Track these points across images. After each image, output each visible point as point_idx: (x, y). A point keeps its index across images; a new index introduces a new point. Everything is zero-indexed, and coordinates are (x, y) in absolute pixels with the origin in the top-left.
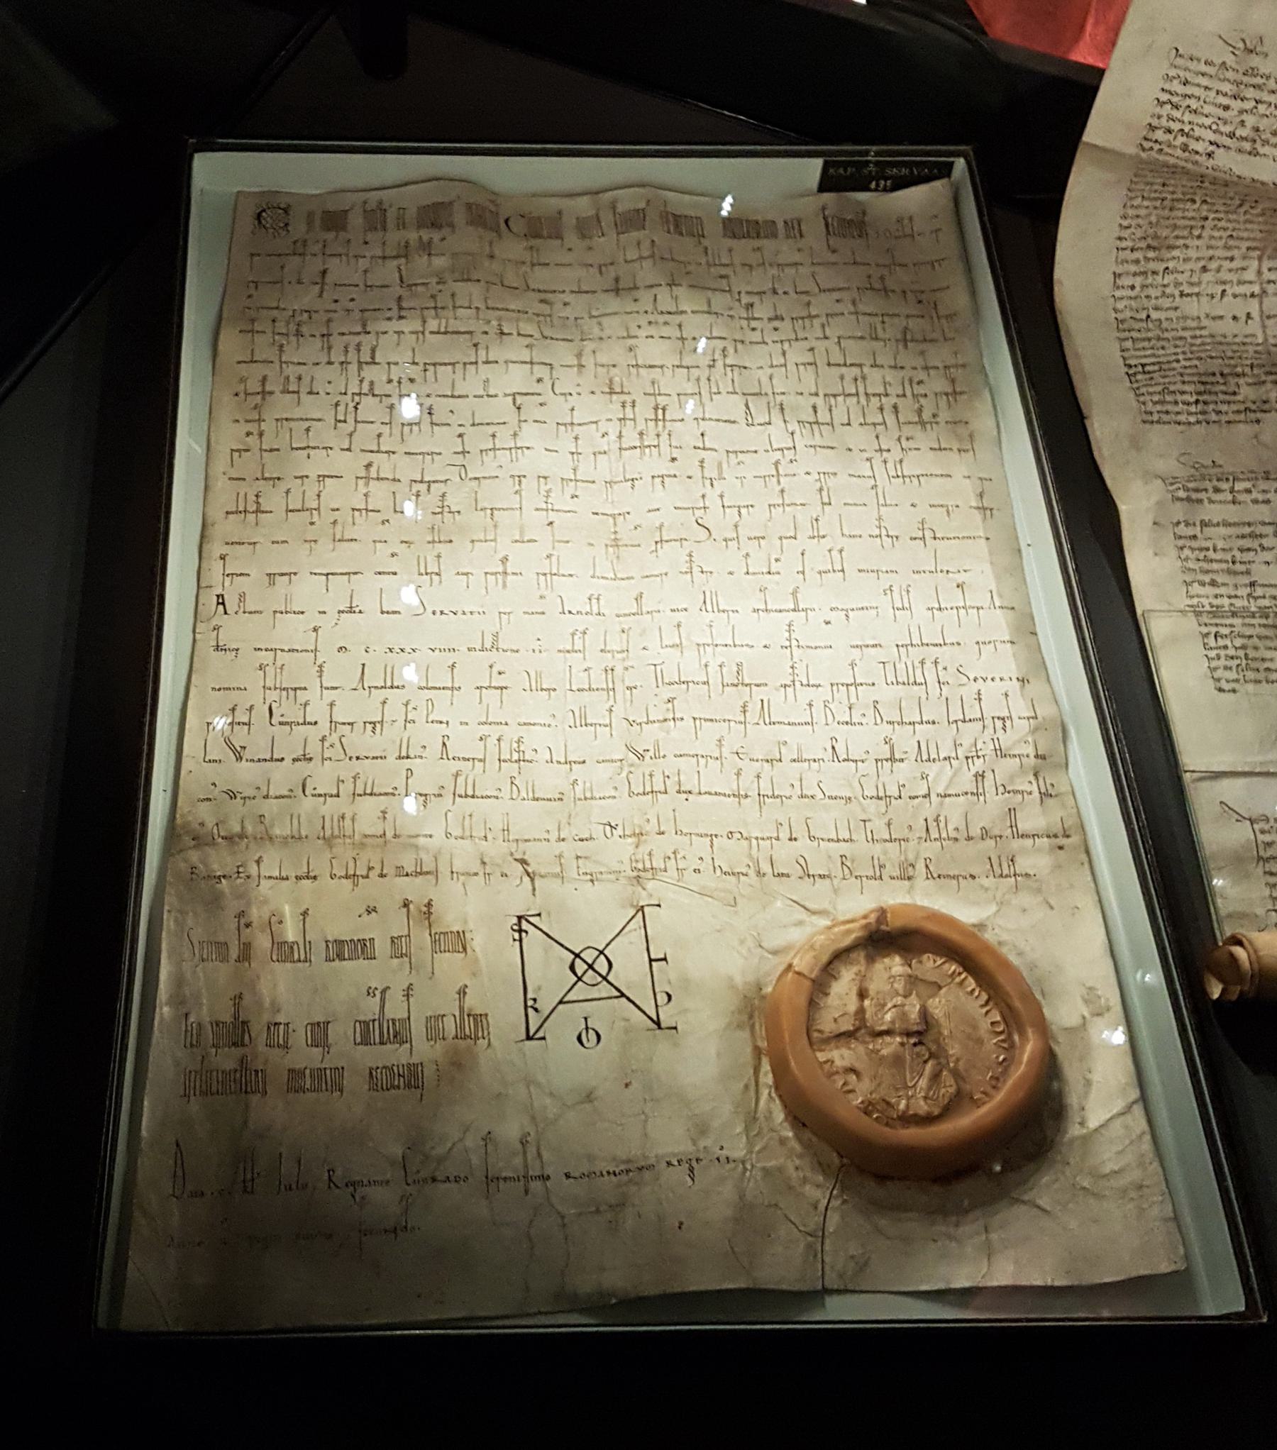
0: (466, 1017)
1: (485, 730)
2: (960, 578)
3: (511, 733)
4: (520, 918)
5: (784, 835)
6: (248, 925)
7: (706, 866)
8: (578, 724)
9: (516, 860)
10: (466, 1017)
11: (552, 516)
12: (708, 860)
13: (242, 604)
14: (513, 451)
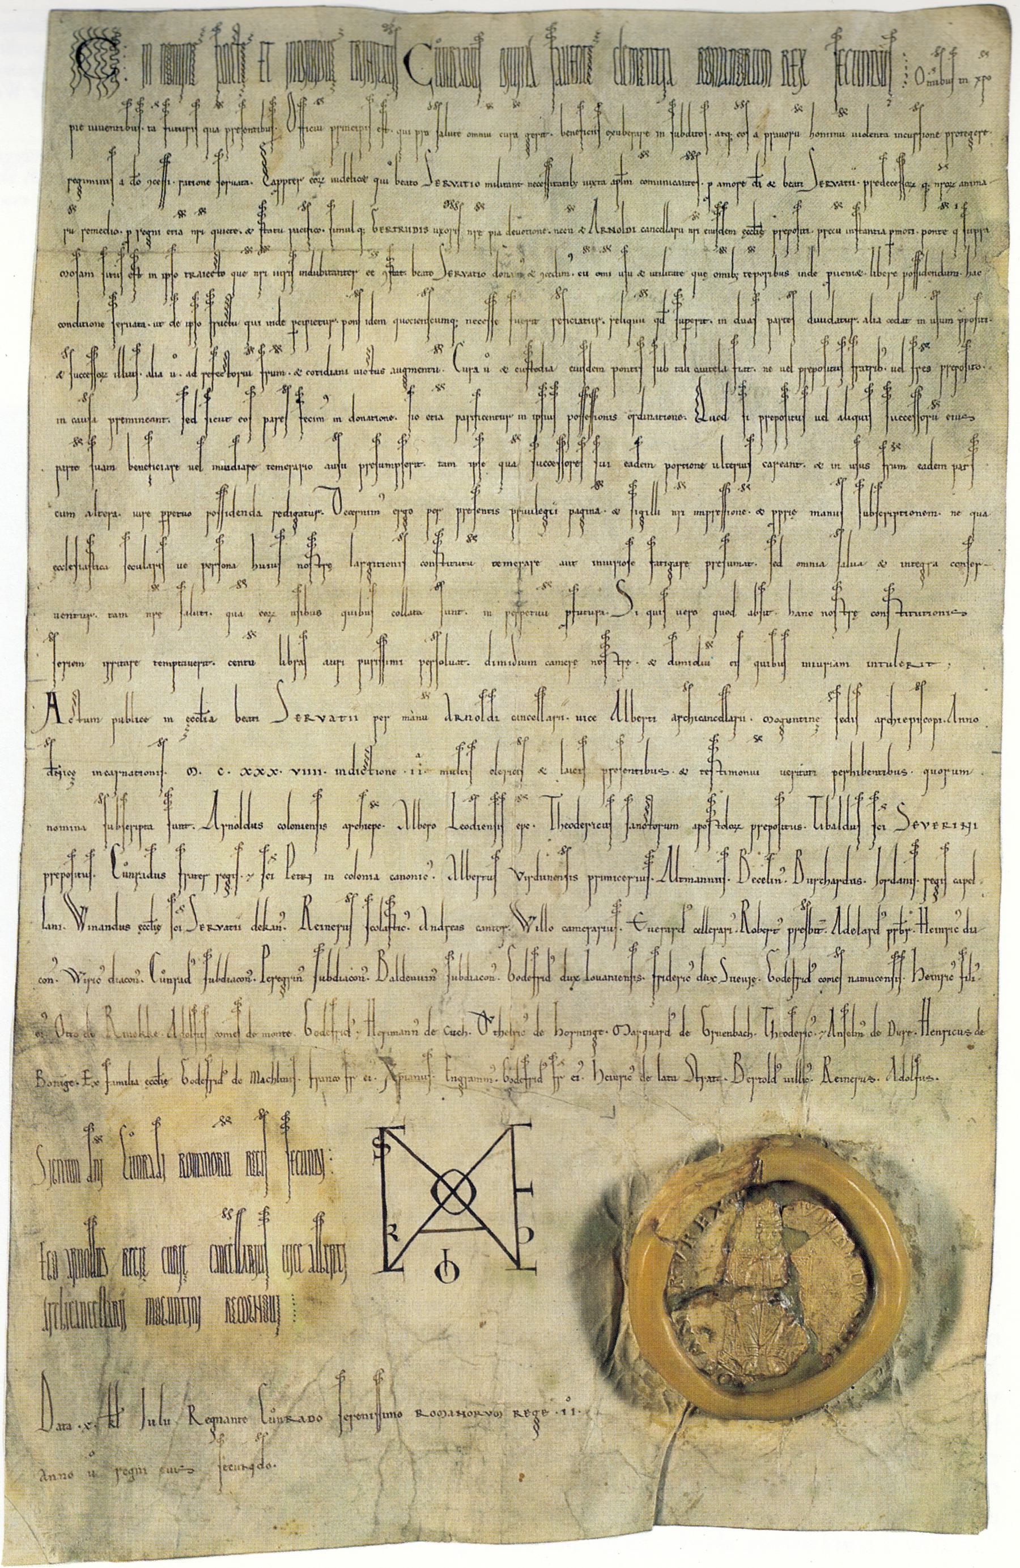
0: (323, 1248)
1: (354, 885)
2: (921, 674)
3: (382, 890)
4: (382, 1130)
5: (676, 1028)
6: (98, 1140)
7: (587, 1071)
8: (458, 875)
9: (381, 1058)
10: (323, 1248)
11: (444, 574)
12: (589, 1064)
13: (76, 709)
14: (400, 469)
